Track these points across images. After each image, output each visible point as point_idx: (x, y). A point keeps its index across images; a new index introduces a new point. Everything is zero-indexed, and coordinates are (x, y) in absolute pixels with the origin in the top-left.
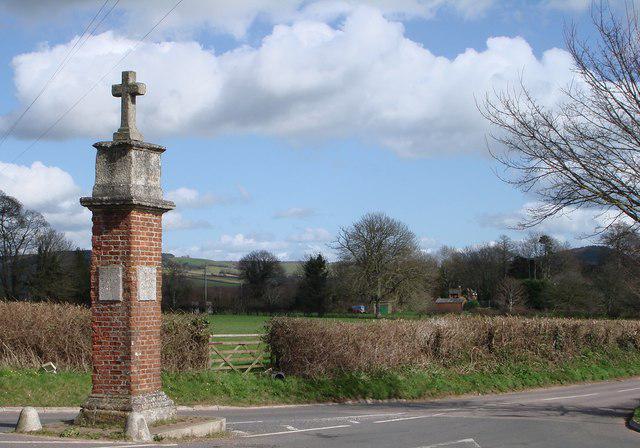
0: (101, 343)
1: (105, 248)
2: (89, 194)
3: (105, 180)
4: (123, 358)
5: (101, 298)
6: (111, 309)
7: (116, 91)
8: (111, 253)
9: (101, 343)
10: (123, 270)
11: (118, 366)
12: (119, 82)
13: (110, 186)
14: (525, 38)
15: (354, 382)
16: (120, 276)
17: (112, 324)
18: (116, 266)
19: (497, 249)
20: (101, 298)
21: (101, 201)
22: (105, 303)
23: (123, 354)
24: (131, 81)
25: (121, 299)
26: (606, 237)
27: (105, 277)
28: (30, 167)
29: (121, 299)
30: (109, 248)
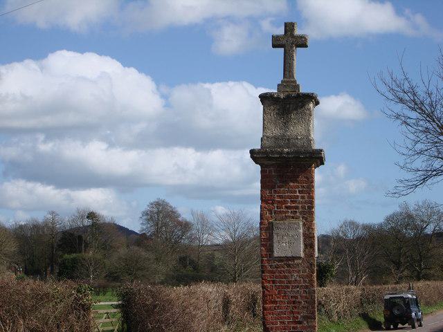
0: (275, 302)
1: (279, 202)
2: (258, 147)
3: (277, 132)
4: (306, 318)
5: (276, 254)
6: (289, 266)
7: (277, 42)
8: (287, 207)
9: (275, 302)
10: (304, 225)
11: (298, 326)
12: (281, 31)
13: (283, 137)
14: (6, 230)
15: (139, 245)
16: (301, 231)
17: (290, 282)
18: (294, 221)
19: (46, 224)
20: (276, 254)
21: (281, 153)
22: (280, 259)
23: (304, 313)
24: (297, 32)
25: (302, 255)
26: (147, 214)
27: (282, 232)
28: (256, 88)
29: (302, 255)
30: (285, 202)
